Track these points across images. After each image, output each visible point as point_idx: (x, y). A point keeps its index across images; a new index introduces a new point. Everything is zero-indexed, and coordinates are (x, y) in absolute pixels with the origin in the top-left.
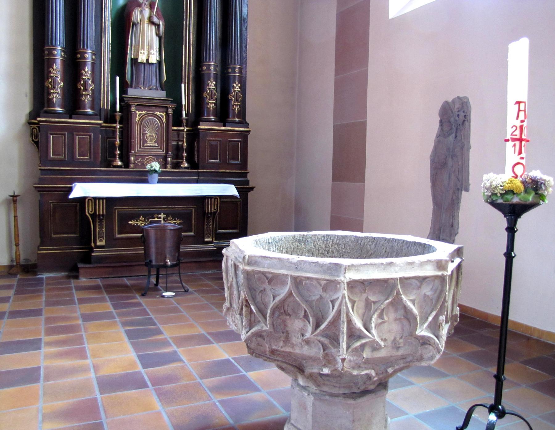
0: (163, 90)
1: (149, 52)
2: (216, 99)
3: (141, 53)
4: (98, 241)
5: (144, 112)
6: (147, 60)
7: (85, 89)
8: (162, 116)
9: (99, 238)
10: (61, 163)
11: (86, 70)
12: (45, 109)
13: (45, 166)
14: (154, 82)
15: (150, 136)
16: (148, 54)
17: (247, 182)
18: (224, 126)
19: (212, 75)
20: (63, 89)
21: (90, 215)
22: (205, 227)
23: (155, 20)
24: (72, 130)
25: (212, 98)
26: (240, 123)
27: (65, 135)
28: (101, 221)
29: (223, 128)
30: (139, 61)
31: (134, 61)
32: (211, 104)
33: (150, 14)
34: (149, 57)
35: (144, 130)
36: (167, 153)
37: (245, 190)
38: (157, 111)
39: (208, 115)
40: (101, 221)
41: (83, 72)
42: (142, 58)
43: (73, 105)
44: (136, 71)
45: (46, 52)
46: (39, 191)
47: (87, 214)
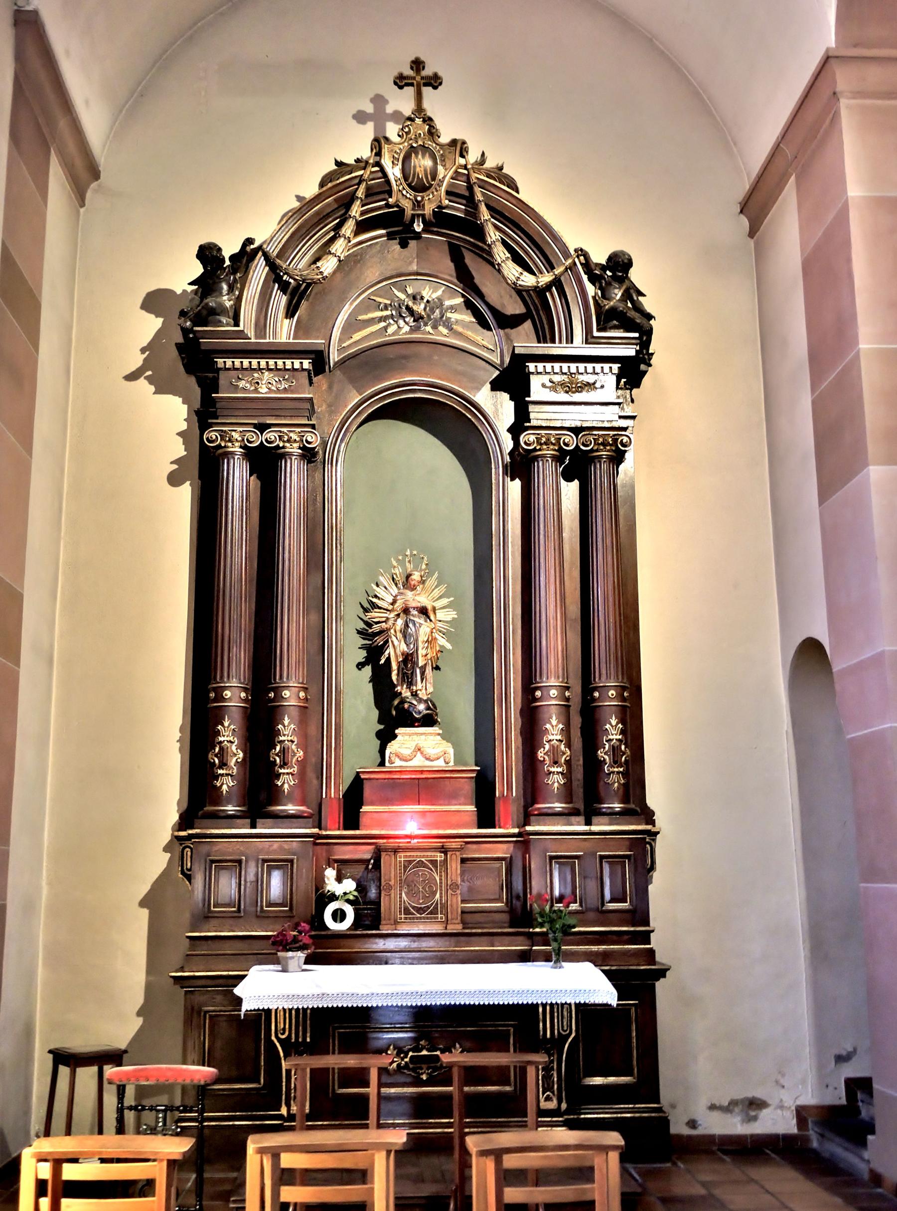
2: (568, 763)
7: (223, 764)
11: (286, 722)
20: (241, 764)
25: (556, 763)
26: (624, 813)
29: (587, 828)
37: (638, 980)
43: (260, 797)
45: (212, 695)
47: (273, 1038)
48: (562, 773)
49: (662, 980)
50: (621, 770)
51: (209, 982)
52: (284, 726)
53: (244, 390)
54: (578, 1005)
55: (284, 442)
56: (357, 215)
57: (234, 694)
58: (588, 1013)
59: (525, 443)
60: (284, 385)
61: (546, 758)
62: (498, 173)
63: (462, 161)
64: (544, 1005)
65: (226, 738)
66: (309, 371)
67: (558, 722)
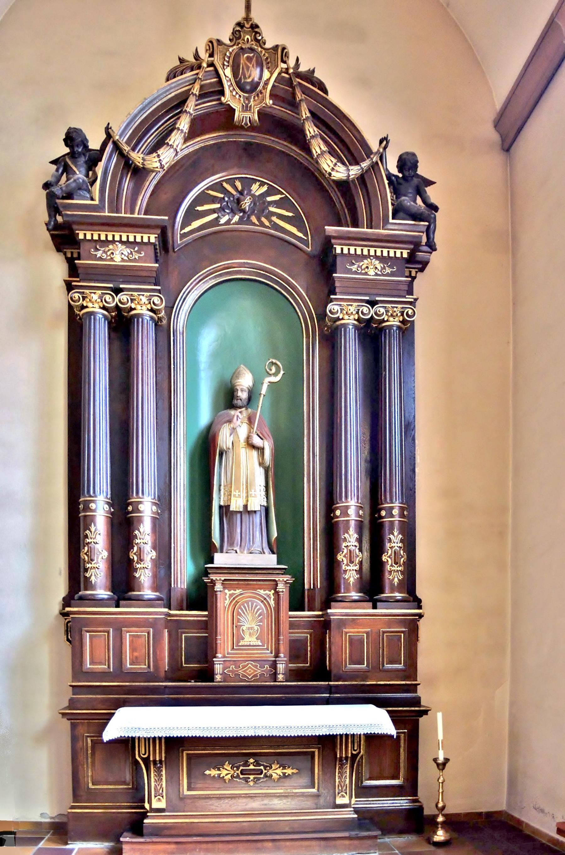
0: (273, 553)
1: (247, 492)
3: (235, 496)
4: (154, 800)
5: (238, 592)
6: (246, 506)
7: (141, 560)
8: (269, 596)
9: (155, 797)
10: (104, 675)
12: (80, 593)
13: (79, 681)
14: (259, 540)
15: (249, 629)
16: (247, 497)
17: (417, 702)
18: (375, 607)
19: (352, 524)
21: (143, 759)
22: (337, 780)
23: (256, 441)
24: (119, 627)
25: (352, 562)
27: (108, 632)
28: (159, 771)
30: (231, 509)
31: (225, 510)
32: (350, 574)
33: (250, 432)
34: (247, 501)
35: (239, 620)
36: (277, 656)
37: (409, 716)
38: (260, 589)
39: (348, 591)
40: (159, 771)
41: (137, 532)
42: (236, 505)
43: (123, 583)
44: (229, 524)
45: (81, 506)
46: (68, 719)
48: (356, 570)
49: (424, 716)
50: (399, 569)
51: (407, 714)
52: (91, 532)
53: (101, 259)
54: (166, 738)
55: (389, 316)
56: (191, 112)
57: (100, 508)
58: (373, 739)
59: (330, 311)
60: (388, 270)
61: (344, 559)
62: (309, 77)
63: (284, 66)
64: (341, 736)
65: (351, 544)
66: (154, 244)
67: (399, 533)
